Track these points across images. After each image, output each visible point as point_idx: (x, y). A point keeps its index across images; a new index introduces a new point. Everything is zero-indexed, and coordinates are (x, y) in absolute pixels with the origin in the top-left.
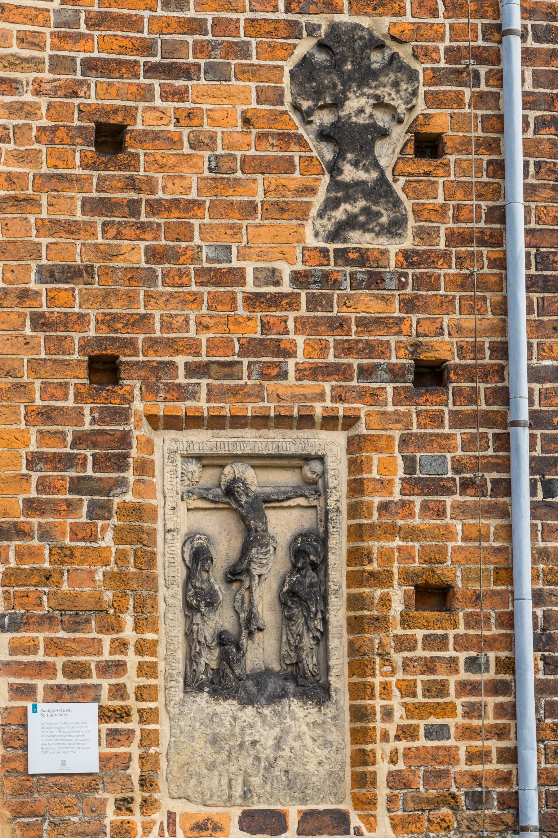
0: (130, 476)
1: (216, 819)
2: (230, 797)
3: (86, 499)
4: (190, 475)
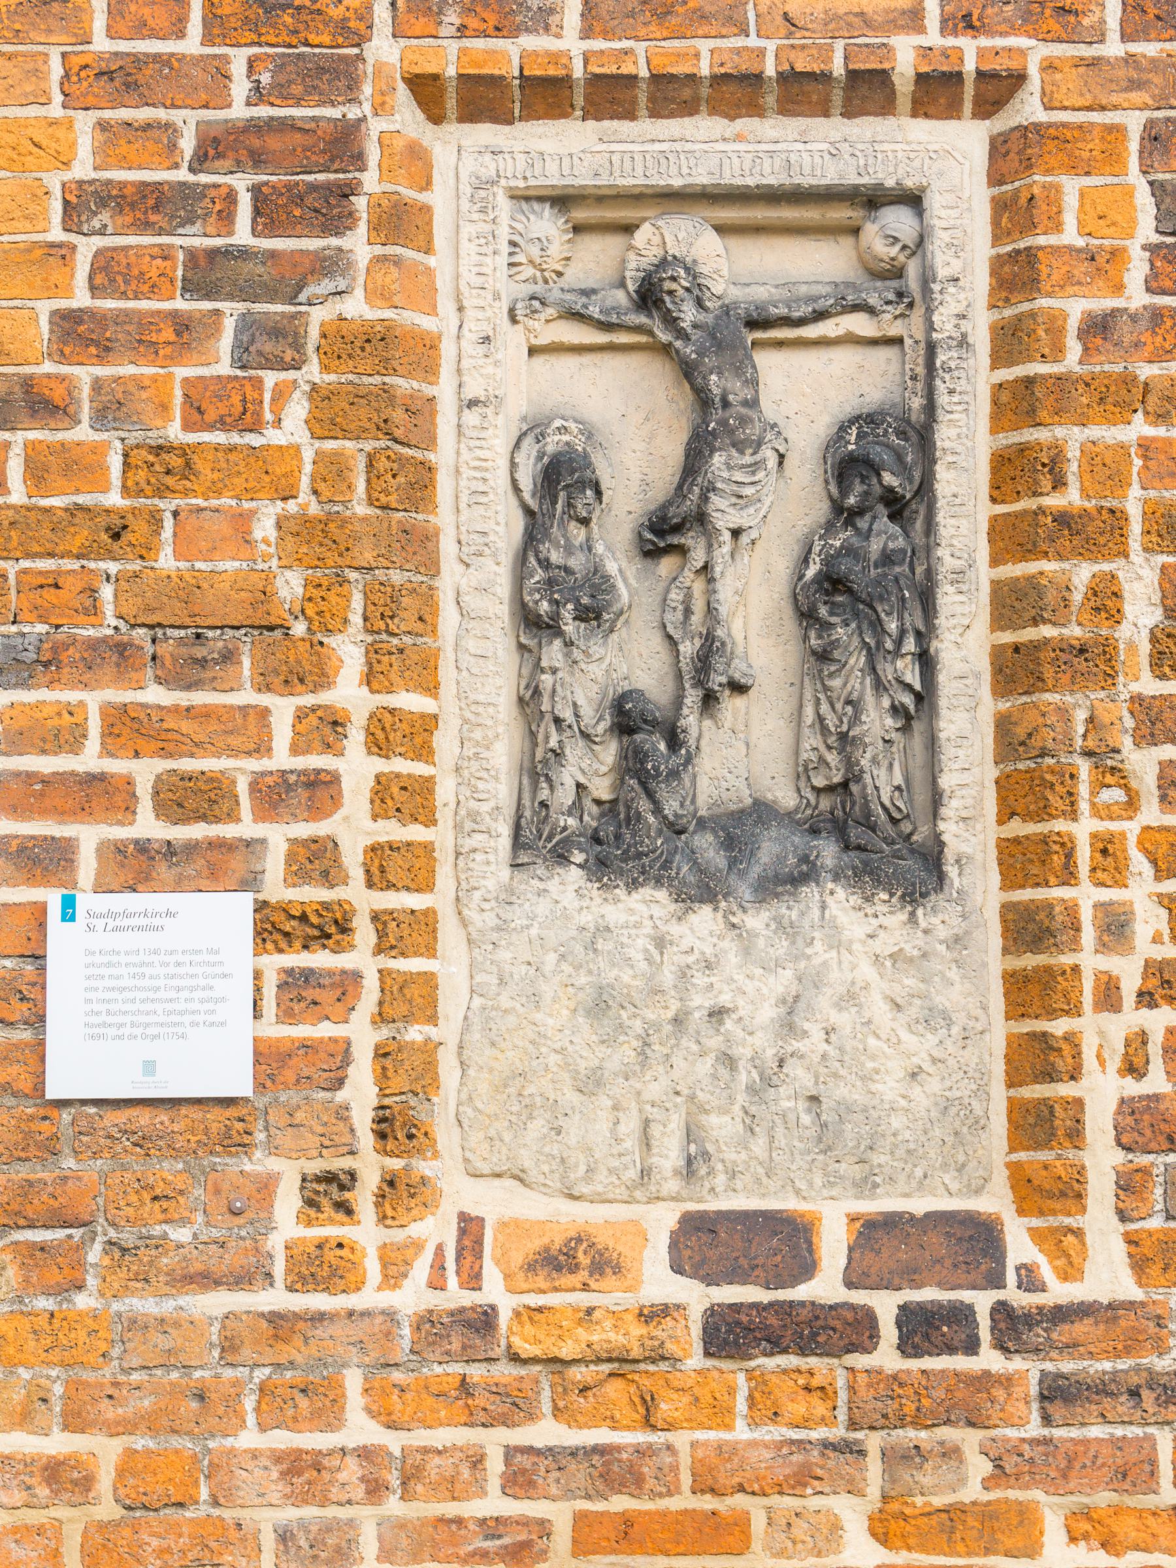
0: (358, 244)
1: (603, 1239)
2: (645, 1173)
3: (231, 310)
4: (535, 251)
